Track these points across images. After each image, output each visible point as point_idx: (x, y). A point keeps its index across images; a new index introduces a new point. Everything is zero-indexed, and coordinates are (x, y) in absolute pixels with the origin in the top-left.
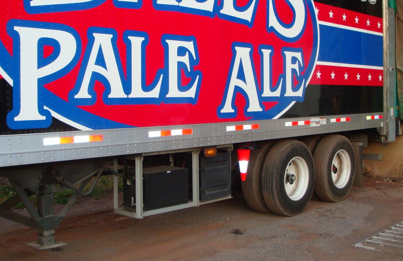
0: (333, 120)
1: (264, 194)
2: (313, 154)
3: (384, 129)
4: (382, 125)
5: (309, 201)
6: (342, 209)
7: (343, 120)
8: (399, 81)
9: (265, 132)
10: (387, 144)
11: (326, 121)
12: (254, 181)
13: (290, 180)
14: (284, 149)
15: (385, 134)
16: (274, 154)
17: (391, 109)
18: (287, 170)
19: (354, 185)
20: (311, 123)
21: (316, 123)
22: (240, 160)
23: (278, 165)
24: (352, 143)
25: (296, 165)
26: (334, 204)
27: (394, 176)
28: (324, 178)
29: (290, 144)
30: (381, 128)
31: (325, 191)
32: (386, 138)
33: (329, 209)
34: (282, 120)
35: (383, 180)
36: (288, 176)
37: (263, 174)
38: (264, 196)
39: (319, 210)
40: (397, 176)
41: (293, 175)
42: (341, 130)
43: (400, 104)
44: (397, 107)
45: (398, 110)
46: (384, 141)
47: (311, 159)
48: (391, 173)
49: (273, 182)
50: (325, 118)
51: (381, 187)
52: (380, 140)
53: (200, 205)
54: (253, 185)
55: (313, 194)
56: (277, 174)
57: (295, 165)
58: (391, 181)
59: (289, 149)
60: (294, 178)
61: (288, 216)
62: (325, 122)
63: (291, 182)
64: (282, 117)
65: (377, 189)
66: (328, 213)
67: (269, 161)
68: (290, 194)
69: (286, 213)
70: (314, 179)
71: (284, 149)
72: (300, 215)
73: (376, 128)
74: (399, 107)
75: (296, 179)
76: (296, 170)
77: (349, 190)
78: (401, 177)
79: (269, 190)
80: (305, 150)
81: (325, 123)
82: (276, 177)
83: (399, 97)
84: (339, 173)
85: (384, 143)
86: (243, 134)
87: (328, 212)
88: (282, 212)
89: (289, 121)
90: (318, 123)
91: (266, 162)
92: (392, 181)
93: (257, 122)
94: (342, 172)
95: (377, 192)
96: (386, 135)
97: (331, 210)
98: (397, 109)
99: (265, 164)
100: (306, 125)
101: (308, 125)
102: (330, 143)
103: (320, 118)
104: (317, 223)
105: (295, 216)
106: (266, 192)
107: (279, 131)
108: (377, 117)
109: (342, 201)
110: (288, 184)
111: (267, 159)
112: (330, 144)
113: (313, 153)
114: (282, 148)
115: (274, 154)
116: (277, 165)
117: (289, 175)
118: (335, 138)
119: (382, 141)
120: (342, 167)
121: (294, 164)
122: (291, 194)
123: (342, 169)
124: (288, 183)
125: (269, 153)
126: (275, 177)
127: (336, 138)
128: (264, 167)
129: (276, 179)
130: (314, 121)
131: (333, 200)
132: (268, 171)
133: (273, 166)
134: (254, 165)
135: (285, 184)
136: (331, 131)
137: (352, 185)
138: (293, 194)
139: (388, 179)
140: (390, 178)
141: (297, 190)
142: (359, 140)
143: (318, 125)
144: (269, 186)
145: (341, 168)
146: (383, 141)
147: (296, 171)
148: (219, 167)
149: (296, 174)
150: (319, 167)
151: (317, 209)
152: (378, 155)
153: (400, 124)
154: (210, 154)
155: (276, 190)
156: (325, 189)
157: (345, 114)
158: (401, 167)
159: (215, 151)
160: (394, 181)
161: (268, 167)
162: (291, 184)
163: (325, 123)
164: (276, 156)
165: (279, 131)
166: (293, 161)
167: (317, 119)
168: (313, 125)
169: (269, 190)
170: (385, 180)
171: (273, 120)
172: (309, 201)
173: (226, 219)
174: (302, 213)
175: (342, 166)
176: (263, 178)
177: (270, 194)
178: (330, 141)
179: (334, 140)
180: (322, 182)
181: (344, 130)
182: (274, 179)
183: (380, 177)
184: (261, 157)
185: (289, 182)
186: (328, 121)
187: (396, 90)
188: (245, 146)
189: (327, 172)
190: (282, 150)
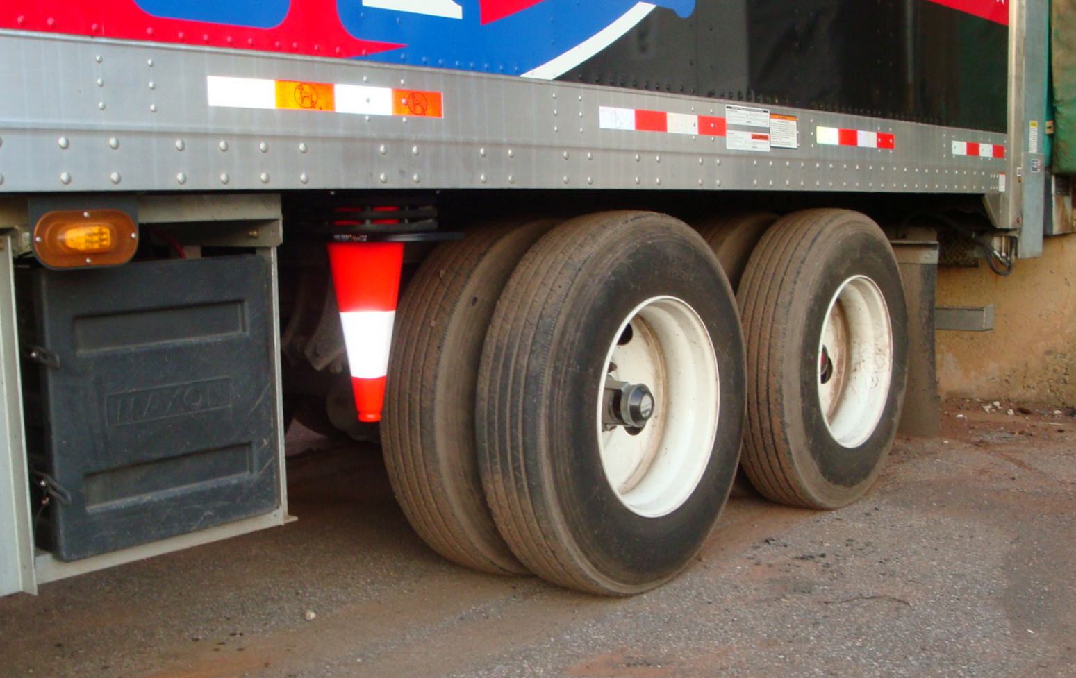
0: (828, 135)
1: (489, 488)
2: (736, 283)
3: (1006, 201)
4: (1002, 188)
5: (725, 503)
6: (868, 544)
7: (867, 139)
8: (1061, 17)
9: (483, 144)
10: (1001, 269)
11: (796, 132)
12: (439, 420)
13: (626, 415)
14: (591, 249)
15: (1010, 226)
16: (540, 280)
17: (1031, 127)
18: (612, 367)
19: (901, 430)
20: (728, 132)
21: (755, 137)
22: (342, 311)
23: (563, 334)
24: (896, 253)
25: (651, 329)
26: (825, 518)
27: (1018, 393)
28: (785, 403)
29: (626, 226)
30: (997, 196)
31: (792, 462)
32: (1013, 242)
33: (812, 549)
34: (582, 91)
35: (978, 407)
36: (616, 397)
37: (483, 387)
38: (491, 499)
39: (765, 553)
40: (1032, 394)
41: (642, 390)
42: (856, 186)
43: (1060, 109)
44: (1048, 124)
45: (1051, 137)
46: (1004, 254)
47: (728, 301)
48: (1007, 381)
49: (536, 426)
50: (793, 117)
51: (988, 438)
52: (989, 250)
53: (43, 588)
54: (433, 442)
55: (736, 482)
56: (554, 381)
57: (652, 341)
58: (1011, 412)
59: (620, 252)
60: (645, 403)
61: (618, 597)
62: (795, 138)
63: (632, 424)
64: (582, 74)
65: (978, 445)
66: (808, 571)
67: (512, 316)
68: (629, 478)
69: (607, 584)
70: (742, 413)
71: (591, 249)
72: (676, 584)
73: (982, 195)
74: (1055, 123)
75: (659, 409)
76: (654, 363)
77: (885, 454)
78: (1047, 396)
79: (516, 469)
80: (703, 262)
81: (793, 143)
82: (551, 398)
83: (1056, 85)
84: (838, 381)
85: (1003, 260)
86: (335, 139)
87: (810, 563)
88: (585, 577)
89: (618, 104)
90: (761, 134)
91: (497, 321)
92: (1015, 414)
93: (430, 79)
94: (853, 375)
95: (982, 458)
96: (1014, 230)
97: (823, 556)
98: (1048, 131)
99: (494, 333)
100: (705, 136)
101: (717, 137)
102: (814, 241)
103: (773, 115)
104: (769, 643)
105: (652, 594)
106: (498, 477)
107: (564, 148)
108: (986, 150)
109: (857, 501)
110: (615, 431)
111: (503, 306)
112: (810, 248)
113: (736, 282)
114: (581, 246)
115: (540, 280)
116: (557, 333)
117: (623, 389)
118: (831, 221)
119: (996, 256)
120: (855, 356)
121: (644, 336)
122: (632, 483)
123: (854, 362)
124: (620, 429)
125: (521, 269)
126: (545, 401)
127: (836, 223)
128: (490, 349)
129: (551, 407)
130: (744, 122)
131: (818, 498)
132: (506, 367)
133: (533, 344)
134: (442, 340)
135: (602, 436)
136: (818, 186)
137: (894, 432)
138: (633, 489)
139: (997, 404)
140: (1007, 402)
141: (662, 461)
142: (921, 242)
143: (763, 146)
144: (514, 448)
145: (849, 358)
146: (1000, 253)
147: (657, 371)
148: (180, 342)
149: (657, 385)
150: (764, 353)
151: (756, 548)
152: (981, 310)
153: (1056, 191)
154: (83, 247)
155: (555, 471)
156: (790, 453)
157: (872, 115)
158: (1049, 358)
159: (119, 235)
160: (1024, 412)
161: (509, 347)
162: (634, 431)
163: (793, 143)
164: (551, 290)
165: (564, 148)
166: (639, 317)
167: (757, 116)
168: (738, 141)
169: (516, 469)
170: (987, 408)
171: (528, 81)
172: (725, 503)
173: (303, 615)
174: (687, 569)
175: (855, 351)
176: (483, 406)
177: (520, 489)
178: (810, 236)
179: (828, 230)
180: (776, 420)
181: (872, 187)
182: (543, 411)
183: (963, 399)
184: (475, 300)
185: (623, 423)
186: (806, 136)
187: (1046, 53)
188: (368, 225)
189: (801, 376)
190: (584, 257)
